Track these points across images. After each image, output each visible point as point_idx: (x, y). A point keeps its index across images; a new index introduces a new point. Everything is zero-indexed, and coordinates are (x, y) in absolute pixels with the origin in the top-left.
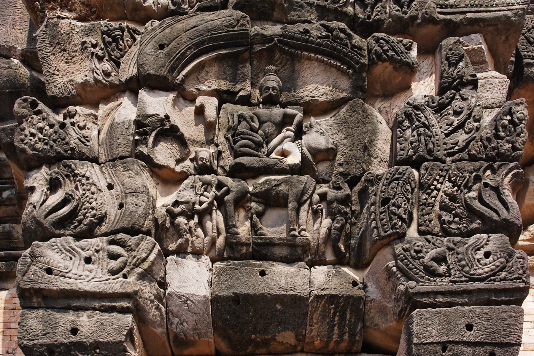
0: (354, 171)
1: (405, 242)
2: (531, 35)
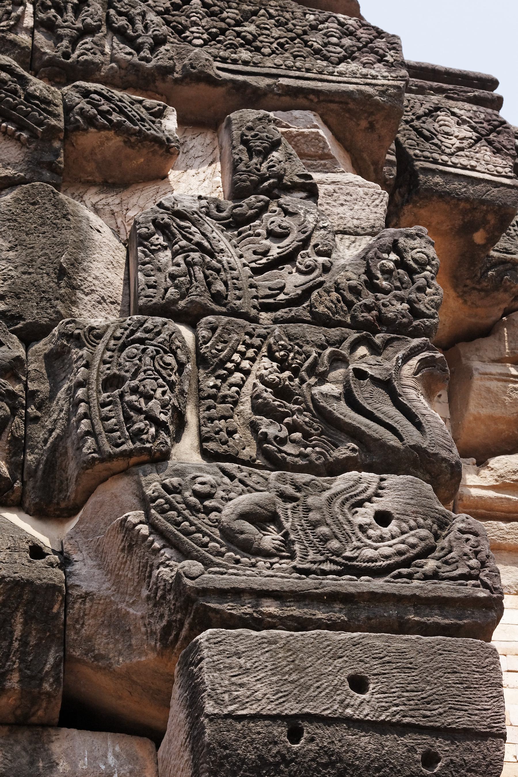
0: (33, 314)
1: (167, 472)
2: (425, 126)
